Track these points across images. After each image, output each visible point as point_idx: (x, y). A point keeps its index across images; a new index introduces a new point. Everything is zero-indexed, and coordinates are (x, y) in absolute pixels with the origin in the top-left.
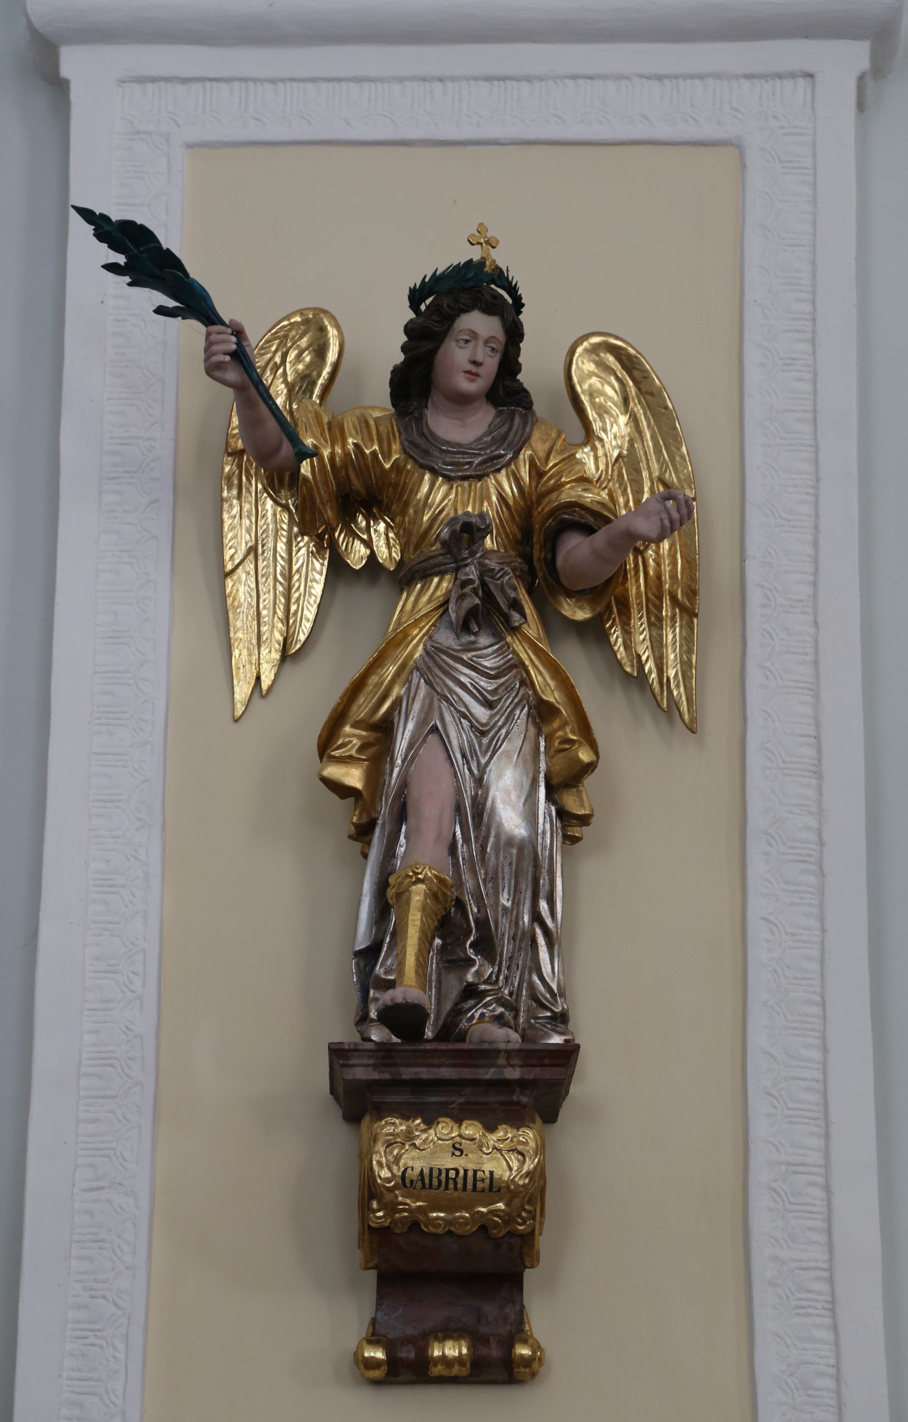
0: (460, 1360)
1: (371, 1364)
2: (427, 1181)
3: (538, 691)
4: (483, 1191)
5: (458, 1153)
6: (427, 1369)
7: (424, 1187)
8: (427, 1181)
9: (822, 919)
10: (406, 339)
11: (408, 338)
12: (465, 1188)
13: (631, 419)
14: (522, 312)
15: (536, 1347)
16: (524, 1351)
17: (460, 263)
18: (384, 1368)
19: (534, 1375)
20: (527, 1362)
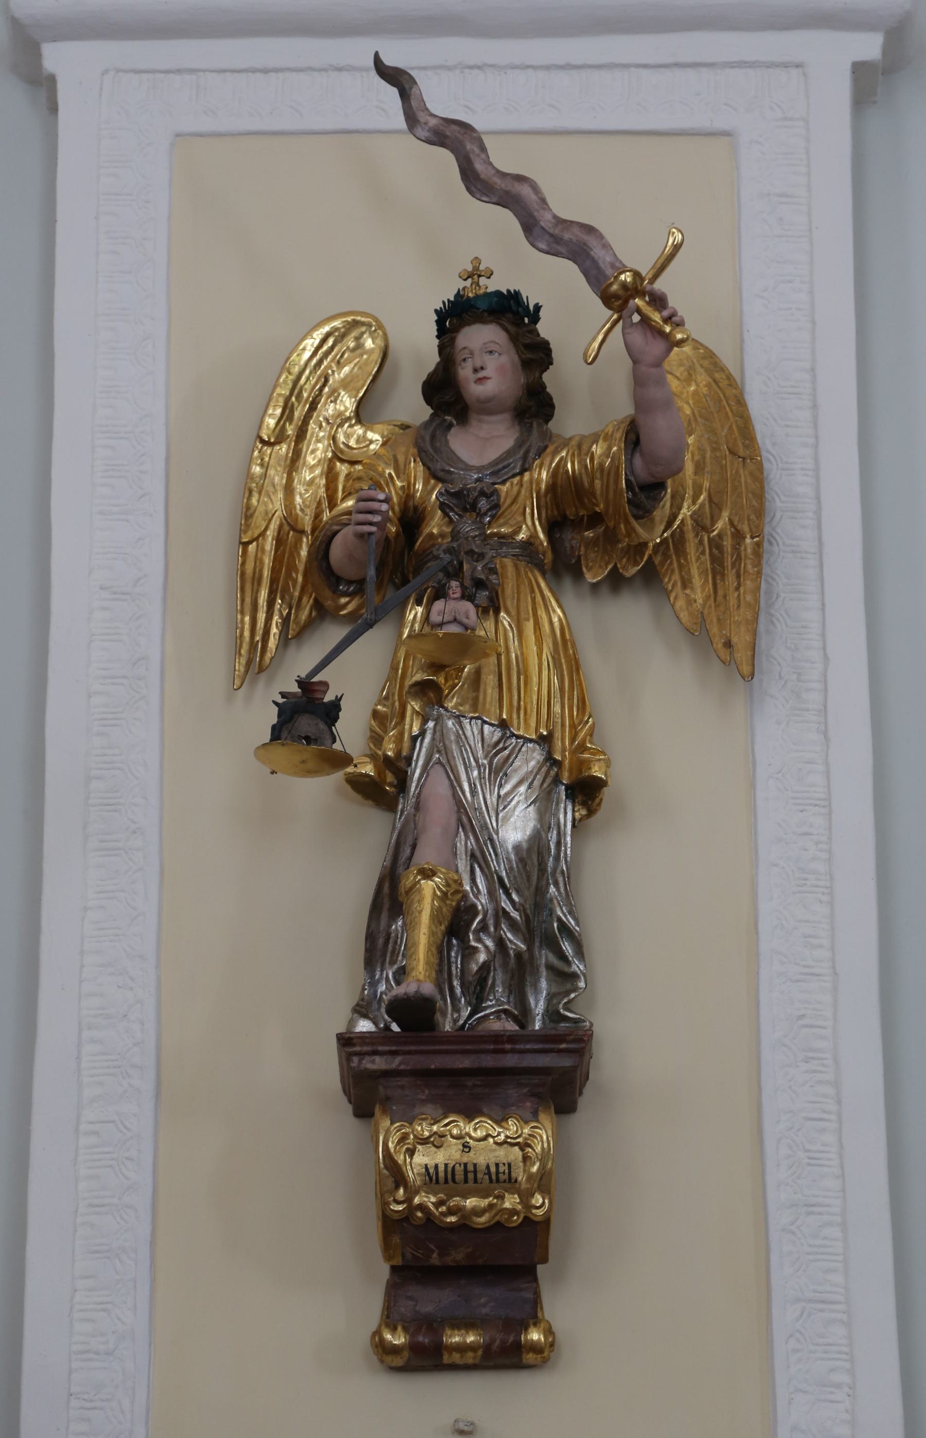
0: (472, 1348)
1: (394, 1350)
2: (494, 1177)
3: (565, 689)
4: (505, 1181)
5: (467, 1150)
6: (441, 1356)
7: (491, 1180)
8: (494, 1177)
9: (825, 733)
10: (432, 411)
11: (432, 408)
12: (446, 1181)
13: (772, 514)
14: (515, 291)
15: (549, 1331)
16: (535, 1336)
17: (459, 289)
18: (406, 1354)
19: (545, 1361)
20: (535, 1348)
